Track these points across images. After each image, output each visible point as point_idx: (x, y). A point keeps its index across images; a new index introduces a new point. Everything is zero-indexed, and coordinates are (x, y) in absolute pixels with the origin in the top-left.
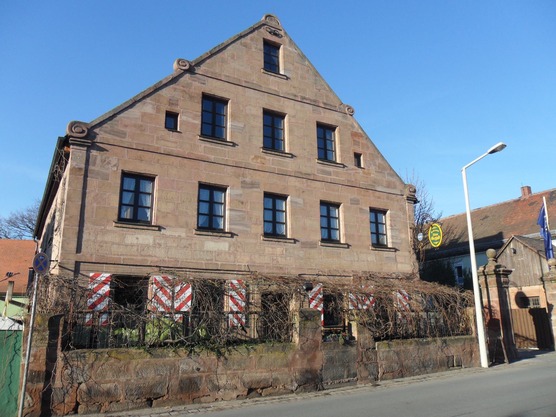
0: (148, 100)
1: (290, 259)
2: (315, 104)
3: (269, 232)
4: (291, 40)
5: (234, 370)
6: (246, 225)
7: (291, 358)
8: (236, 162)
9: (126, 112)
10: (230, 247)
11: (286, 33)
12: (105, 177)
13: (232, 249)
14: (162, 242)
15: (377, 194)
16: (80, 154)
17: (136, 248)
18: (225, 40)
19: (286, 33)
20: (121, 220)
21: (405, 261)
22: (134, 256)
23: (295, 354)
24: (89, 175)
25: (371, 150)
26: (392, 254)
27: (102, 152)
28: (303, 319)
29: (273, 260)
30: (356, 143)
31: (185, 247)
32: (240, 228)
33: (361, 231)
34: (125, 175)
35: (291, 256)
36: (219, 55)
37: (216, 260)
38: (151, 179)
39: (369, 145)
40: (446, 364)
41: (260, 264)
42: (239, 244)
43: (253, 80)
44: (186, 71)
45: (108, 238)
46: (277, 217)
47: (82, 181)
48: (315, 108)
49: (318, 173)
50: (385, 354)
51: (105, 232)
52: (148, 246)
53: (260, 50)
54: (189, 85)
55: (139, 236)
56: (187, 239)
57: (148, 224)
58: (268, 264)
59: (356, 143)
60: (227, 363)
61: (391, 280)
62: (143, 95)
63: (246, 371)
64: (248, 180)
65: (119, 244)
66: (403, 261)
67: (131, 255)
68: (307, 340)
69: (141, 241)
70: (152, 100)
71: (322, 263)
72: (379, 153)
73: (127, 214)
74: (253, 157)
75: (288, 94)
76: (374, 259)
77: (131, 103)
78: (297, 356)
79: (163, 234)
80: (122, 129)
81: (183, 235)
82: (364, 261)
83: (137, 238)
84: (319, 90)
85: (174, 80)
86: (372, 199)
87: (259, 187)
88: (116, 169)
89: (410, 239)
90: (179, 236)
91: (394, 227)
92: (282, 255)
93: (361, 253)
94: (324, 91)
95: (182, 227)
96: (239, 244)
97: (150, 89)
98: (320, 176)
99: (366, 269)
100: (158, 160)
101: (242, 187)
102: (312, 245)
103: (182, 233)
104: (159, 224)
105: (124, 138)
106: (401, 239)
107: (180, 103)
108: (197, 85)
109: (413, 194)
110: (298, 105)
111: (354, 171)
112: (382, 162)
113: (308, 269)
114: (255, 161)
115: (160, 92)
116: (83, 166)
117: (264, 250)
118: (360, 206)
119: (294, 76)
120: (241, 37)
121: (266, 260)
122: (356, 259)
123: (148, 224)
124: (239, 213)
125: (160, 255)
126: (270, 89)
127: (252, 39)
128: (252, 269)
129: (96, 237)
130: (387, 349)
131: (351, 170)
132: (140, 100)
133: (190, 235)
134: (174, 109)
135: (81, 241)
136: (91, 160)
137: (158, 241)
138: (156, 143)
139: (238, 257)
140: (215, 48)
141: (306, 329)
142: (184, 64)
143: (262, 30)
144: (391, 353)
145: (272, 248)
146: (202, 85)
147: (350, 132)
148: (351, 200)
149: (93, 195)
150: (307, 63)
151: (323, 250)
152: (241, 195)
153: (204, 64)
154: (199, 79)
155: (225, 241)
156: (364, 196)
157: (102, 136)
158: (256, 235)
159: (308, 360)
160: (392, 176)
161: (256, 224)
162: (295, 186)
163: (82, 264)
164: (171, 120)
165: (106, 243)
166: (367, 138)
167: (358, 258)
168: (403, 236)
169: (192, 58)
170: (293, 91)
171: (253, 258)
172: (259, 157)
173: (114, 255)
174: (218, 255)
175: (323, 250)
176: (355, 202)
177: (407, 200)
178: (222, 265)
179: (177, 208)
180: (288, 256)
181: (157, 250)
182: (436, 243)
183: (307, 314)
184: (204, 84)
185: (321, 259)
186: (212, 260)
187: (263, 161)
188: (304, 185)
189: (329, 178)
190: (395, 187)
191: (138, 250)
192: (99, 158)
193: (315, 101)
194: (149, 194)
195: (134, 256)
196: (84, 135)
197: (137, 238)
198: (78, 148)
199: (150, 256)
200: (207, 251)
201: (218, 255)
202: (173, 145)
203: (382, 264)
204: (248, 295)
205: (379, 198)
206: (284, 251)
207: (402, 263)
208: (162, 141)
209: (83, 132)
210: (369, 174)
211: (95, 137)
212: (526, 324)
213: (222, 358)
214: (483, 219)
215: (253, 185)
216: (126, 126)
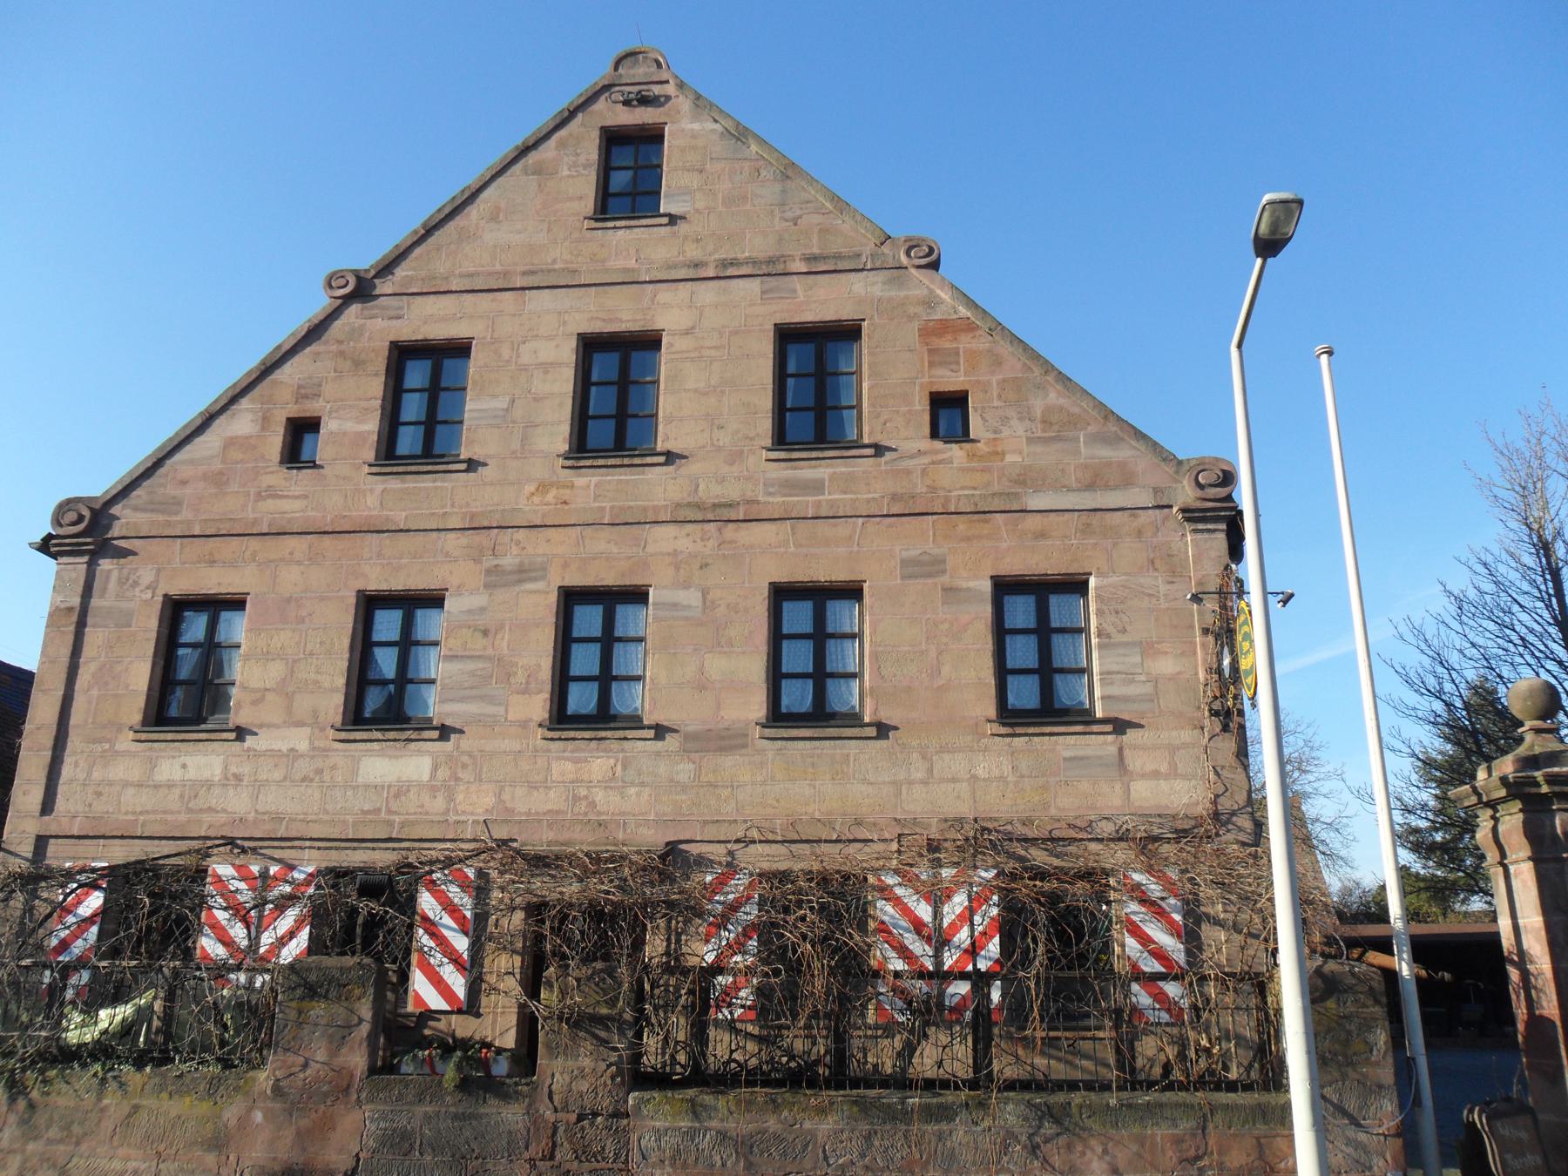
0: (245, 403)
1: (638, 795)
2: (771, 270)
3: (583, 711)
4: (698, 97)
5: (50, 1142)
7: (233, 1122)
9: (188, 448)
10: (435, 768)
11: (681, 85)
12: (125, 620)
13: (443, 773)
14: (246, 769)
15: (1032, 522)
16: (74, 575)
17: (177, 792)
18: (471, 179)
19: (681, 85)
20: (1009, 716)
21: (1173, 766)
22: (172, 813)
23: (250, 1110)
24: (90, 620)
25: (1013, 365)
26: (1101, 745)
27: (122, 561)
28: (299, 992)
29: (576, 799)
30: (937, 358)
31: (303, 780)
32: (473, 708)
33: (946, 670)
34: (1004, 587)
35: (642, 784)
36: (451, 226)
37: (389, 812)
38: (1076, 586)
39: (1004, 348)
41: (529, 814)
42: (465, 759)
43: (554, 262)
44: (348, 300)
45: (120, 771)
47: (70, 638)
49: (770, 494)
50: (669, 1141)
51: (112, 755)
52: (209, 784)
53: (585, 167)
54: (356, 333)
55: (188, 760)
56: (312, 757)
57: (1080, 717)
58: (558, 812)
59: (937, 358)
60: (30, 1118)
61: (1093, 846)
62: (230, 394)
63: (84, 1147)
65: (139, 785)
66: (1164, 768)
67: (165, 812)
68: (305, 1066)
69: (192, 774)
70: (253, 401)
71: (610, 797)
72: (1048, 367)
73: (797, 696)
74: (532, 489)
75: (675, 266)
76: (1007, 769)
77: (199, 422)
78: (258, 1116)
79: (249, 749)
80: (173, 493)
81: (303, 746)
82: (954, 780)
83: (184, 766)
85: (315, 332)
86: (1004, 545)
87: (543, 578)
88: (149, 595)
89: (1202, 675)
90: (292, 750)
91: (1117, 638)
92: (609, 783)
93: (943, 749)
94: (816, 219)
95: (300, 724)
96: (465, 759)
97: (249, 373)
99: (965, 809)
100: (254, 554)
101: (486, 586)
102: (724, 741)
103: (299, 740)
104: (886, 716)
105: (176, 513)
106: (1155, 681)
107: (328, 390)
108: (374, 329)
109: (1221, 492)
110: (707, 293)
111: (925, 460)
112: (1062, 401)
113: (705, 822)
114: (536, 499)
115: (278, 375)
116: (76, 601)
117: (549, 769)
118: (945, 579)
119: (700, 205)
120: (525, 150)
121: (553, 800)
123: (1080, 717)
124: (470, 666)
125: (235, 807)
126: (607, 271)
127: (562, 145)
128: (501, 833)
129: (89, 773)
130: (685, 1124)
131: (912, 457)
132: (223, 409)
133: (321, 744)
135: (56, 786)
136: (97, 585)
137: (233, 769)
139: (460, 797)
140: (439, 210)
141: (307, 1029)
142: (342, 281)
143: (601, 105)
144: (706, 1142)
145: (576, 761)
146: (394, 322)
149: (93, 667)
150: (754, 148)
151: (770, 754)
152: (483, 609)
153: (404, 264)
154: (384, 308)
155: (420, 752)
156: (968, 539)
157: (127, 518)
158: (524, 725)
159: (298, 1133)
160: (1111, 441)
163: (52, 841)
165: (111, 784)
166: (997, 328)
167: (930, 771)
168: (1166, 666)
169: (366, 261)
170: (693, 252)
171: (506, 796)
172: (551, 485)
173: (126, 813)
174: (397, 796)
175: (770, 754)
176: (924, 568)
177: (1188, 520)
178: (403, 825)
179: (293, 671)
180: (633, 784)
181: (231, 792)
183: (313, 978)
184: (399, 318)
185: (764, 783)
187: (566, 494)
188: (710, 544)
189: (806, 503)
191: (182, 796)
192: (115, 575)
193: (770, 261)
194: (853, 636)
195: (172, 813)
196: (81, 527)
197: (184, 766)
199: (211, 810)
200: (366, 786)
201: (397, 796)
203: (1045, 788)
204: (481, 918)
205: (1042, 535)
206: (619, 768)
207: (1156, 775)
208: (270, 502)
209: (81, 518)
210: (1000, 455)
211: (109, 527)
213: (21, 1104)
215: (524, 573)
216: (184, 483)
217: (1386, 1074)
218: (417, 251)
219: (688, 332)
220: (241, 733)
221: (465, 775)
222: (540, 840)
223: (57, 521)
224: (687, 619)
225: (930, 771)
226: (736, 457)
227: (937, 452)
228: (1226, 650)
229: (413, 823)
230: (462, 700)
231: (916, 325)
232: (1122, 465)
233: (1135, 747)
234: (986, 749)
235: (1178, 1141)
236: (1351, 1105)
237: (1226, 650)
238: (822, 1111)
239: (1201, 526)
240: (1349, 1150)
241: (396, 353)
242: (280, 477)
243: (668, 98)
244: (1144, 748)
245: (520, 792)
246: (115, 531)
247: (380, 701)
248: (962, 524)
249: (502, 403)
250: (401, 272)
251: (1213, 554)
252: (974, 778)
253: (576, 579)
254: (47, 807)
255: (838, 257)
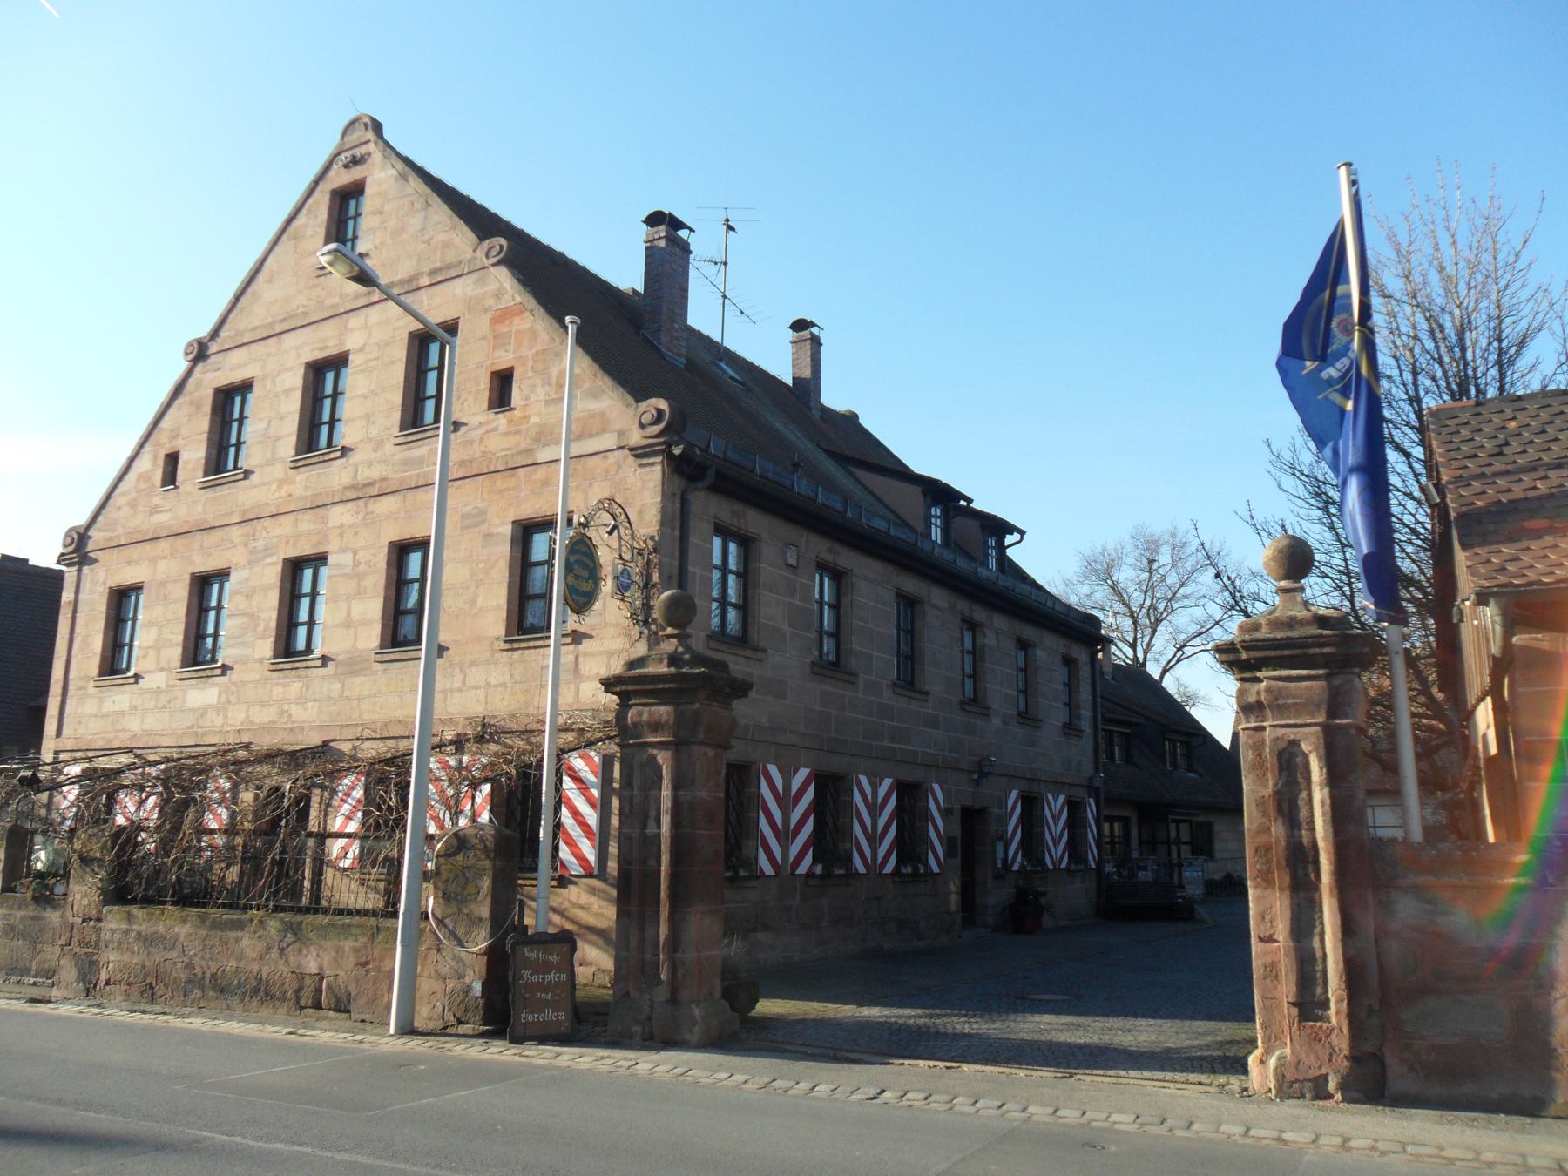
40: (290, 994)
50: (117, 936)
52: (123, 713)
55: (116, 698)
75: (272, 324)
76: (507, 677)
95: (162, 670)
102: (354, 666)
118: (484, 527)
122: (458, 685)
130: (124, 926)
152: (247, 580)
155: (214, 684)
164: (501, 387)
169: (203, 331)
217: (484, 911)
218: (232, 315)
219: (361, 350)
220: (225, 669)
222: (264, 742)
223: (65, 546)
224: (344, 575)
225: (464, 682)
226: (380, 443)
227: (489, 422)
231: (489, 315)
232: (602, 414)
233: (586, 654)
234: (497, 662)
235: (357, 951)
236: (460, 932)
238: (184, 921)
239: (645, 461)
240: (453, 964)
241: (222, 396)
242: (159, 497)
243: (369, 154)
244: (593, 655)
245: (257, 708)
246: (90, 547)
247: (401, 627)
248: (500, 482)
249: (263, 425)
250: (223, 334)
251: (652, 484)
252: (488, 685)
253: (293, 552)
254: (59, 733)
255: (449, 267)
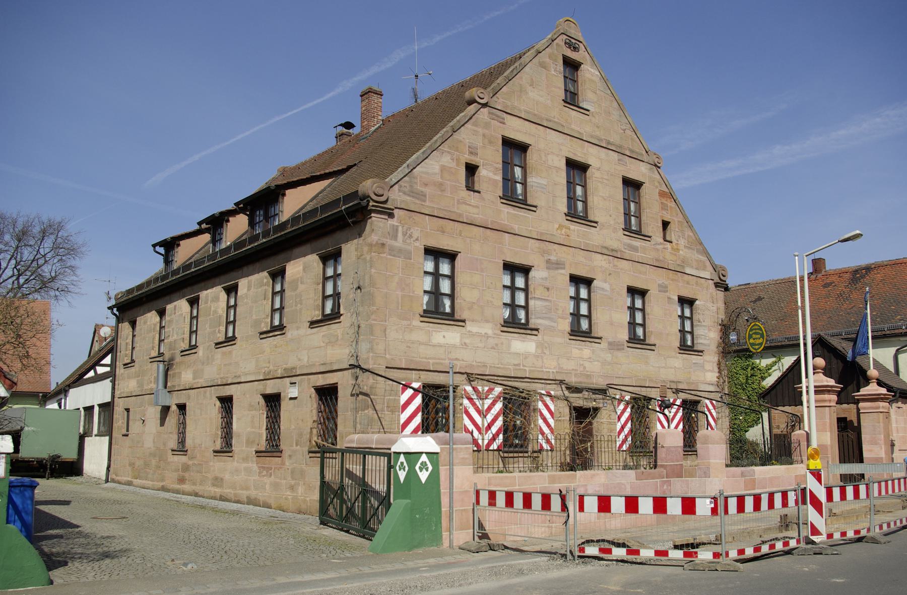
6: (550, 319)
8: (542, 234)
13: (539, 351)
46: (441, 269)
48: (621, 156)
52: (454, 346)
64: (553, 258)
81: (490, 332)
84: (624, 130)
87: (564, 268)
95: (487, 321)
98: (628, 254)
105: (425, 201)
111: (661, 246)
118: (667, 294)
125: (469, 359)
134: (474, 160)
138: (458, 208)
147: (657, 190)
148: (659, 286)
161: (562, 318)
162: (601, 267)
174: (526, 358)
178: (530, 371)
182: (757, 347)
186: (518, 365)
189: (638, 256)
190: (704, 269)
193: (620, 147)
198: (897, 331)
202: (475, 210)
208: (464, 206)
212: (846, 454)
214: (755, 302)
221: (547, 352)
222: (573, 380)
228: (861, 378)
229: (533, 371)
230: (542, 318)
237: (861, 378)
